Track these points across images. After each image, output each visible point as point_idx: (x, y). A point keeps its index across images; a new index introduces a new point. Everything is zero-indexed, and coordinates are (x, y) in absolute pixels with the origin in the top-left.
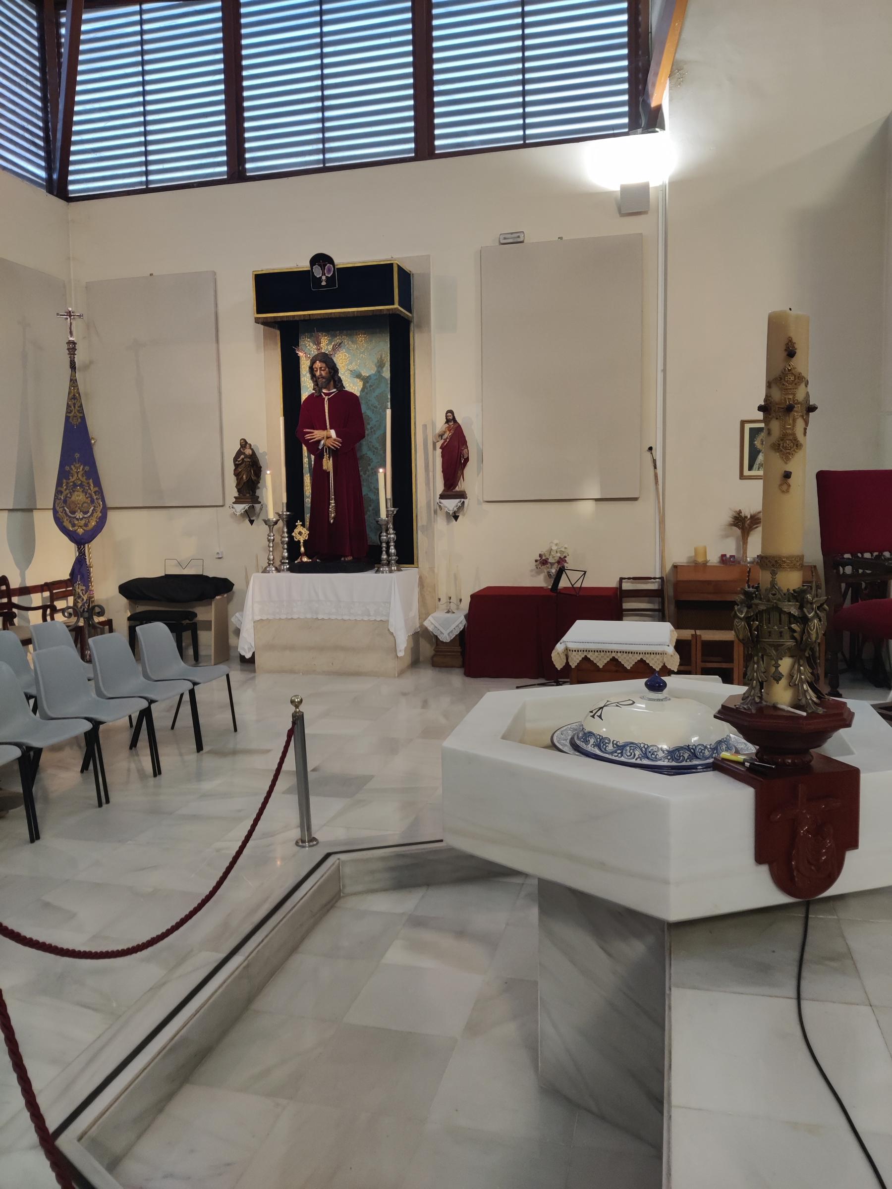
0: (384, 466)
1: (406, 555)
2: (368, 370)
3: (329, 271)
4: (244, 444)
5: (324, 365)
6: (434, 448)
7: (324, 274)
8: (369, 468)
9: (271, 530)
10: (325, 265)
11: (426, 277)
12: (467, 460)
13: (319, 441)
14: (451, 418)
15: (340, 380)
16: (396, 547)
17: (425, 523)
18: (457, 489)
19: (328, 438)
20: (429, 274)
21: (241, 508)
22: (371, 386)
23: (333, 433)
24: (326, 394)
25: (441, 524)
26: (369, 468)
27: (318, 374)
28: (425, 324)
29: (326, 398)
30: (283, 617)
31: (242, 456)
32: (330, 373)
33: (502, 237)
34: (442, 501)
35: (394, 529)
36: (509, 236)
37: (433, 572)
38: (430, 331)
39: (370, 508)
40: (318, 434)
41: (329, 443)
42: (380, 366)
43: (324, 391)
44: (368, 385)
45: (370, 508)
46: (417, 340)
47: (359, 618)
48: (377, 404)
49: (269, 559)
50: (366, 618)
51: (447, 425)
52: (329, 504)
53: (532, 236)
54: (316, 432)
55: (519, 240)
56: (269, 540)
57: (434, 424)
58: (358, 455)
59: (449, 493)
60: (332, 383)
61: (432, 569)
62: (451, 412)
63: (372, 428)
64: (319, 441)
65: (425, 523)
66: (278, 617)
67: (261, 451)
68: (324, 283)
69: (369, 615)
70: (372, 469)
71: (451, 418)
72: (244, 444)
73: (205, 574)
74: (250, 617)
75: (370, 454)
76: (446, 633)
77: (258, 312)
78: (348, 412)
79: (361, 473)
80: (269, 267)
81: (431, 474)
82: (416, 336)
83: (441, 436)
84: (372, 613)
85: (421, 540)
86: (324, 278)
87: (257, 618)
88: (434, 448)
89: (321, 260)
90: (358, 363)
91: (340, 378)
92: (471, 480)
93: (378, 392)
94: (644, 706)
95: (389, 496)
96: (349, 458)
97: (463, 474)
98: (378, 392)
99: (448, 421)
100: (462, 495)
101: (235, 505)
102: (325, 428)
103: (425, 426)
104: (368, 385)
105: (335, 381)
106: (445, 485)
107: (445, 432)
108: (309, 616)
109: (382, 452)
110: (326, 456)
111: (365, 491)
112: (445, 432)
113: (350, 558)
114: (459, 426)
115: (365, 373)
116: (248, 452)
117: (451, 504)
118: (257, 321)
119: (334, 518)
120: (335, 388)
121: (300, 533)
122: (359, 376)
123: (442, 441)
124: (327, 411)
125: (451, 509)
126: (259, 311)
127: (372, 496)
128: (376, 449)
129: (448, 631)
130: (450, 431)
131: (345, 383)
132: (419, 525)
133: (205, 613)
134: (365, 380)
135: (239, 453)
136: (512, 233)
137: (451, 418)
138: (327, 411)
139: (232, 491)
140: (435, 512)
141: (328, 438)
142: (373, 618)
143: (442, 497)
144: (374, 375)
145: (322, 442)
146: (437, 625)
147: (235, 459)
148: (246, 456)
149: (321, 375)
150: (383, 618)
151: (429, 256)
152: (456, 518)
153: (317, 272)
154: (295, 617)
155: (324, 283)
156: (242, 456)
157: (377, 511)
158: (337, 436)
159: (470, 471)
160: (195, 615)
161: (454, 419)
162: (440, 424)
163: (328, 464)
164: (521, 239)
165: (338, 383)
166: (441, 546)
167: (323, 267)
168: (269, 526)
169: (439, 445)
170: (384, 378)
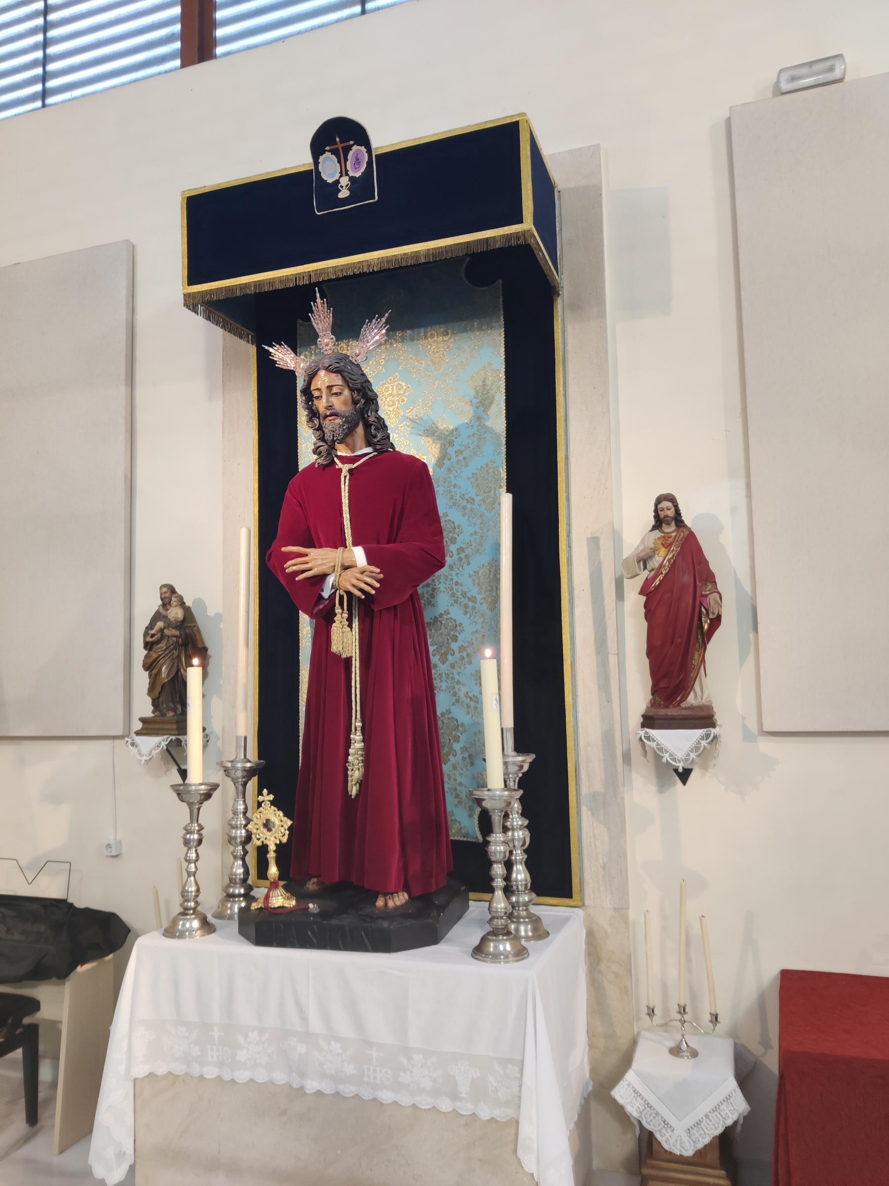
0: (496, 642)
1: (553, 873)
2: (453, 416)
3: (358, 161)
4: (169, 594)
5: (337, 380)
6: (620, 595)
7: (344, 172)
8: (454, 646)
9: (194, 816)
10: (347, 150)
11: (592, 196)
12: (716, 622)
13: (323, 577)
14: (667, 515)
15: (382, 425)
16: (528, 864)
17: (599, 787)
18: (691, 700)
19: (346, 568)
20: (600, 188)
21: (153, 744)
22: (458, 452)
23: (359, 555)
24: (344, 460)
25: (641, 791)
26: (454, 646)
27: (321, 405)
28: (592, 299)
29: (345, 468)
30: (210, 1072)
31: (160, 624)
32: (355, 402)
33: (784, 77)
34: (653, 733)
35: (524, 814)
36: (805, 70)
37: (625, 920)
38: (603, 315)
39: (457, 747)
40: (318, 559)
41: (350, 582)
42: (483, 403)
43: (342, 451)
44: (451, 451)
45: (457, 747)
46: (570, 337)
47: (425, 1102)
48: (472, 492)
49: (184, 894)
50: (445, 1105)
51: (657, 534)
52: (348, 743)
53: (861, 63)
54: (313, 553)
55: (830, 77)
56: (187, 842)
57: (617, 537)
58: (428, 616)
59: (671, 712)
60: (360, 430)
61: (621, 911)
62: (671, 498)
63: (460, 550)
64: (323, 577)
65: (599, 787)
66: (196, 1070)
67: (211, 613)
68: (344, 194)
69: (455, 1096)
70: (462, 648)
71: (671, 513)
72: (169, 594)
73: (70, 900)
74: (122, 1068)
75: (457, 614)
76: (680, 1126)
77: (191, 281)
78: (400, 507)
79: (434, 659)
80: (587, 876)
81: (612, 660)
82: (569, 329)
83: (644, 561)
84: (464, 1089)
85: (588, 832)
86: (345, 181)
87: (141, 1070)
88: (620, 595)
89: (340, 134)
90: (433, 394)
91: (380, 419)
92: (722, 675)
93: (475, 465)
94: (488, 652)
95: (509, 722)
96: (397, 616)
97: (703, 660)
98: (475, 465)
99: (659, 522)
100: (703, 719)
101: (139, 739)
102: (338, 542)
103: (594, 542)
104: (451, 451)
105: (367, 426)
106: (656, 690)
107: (654, 551)
108: (280, 1077)
109: (485, 607)
110: (341, 616)
111: (442, 702)
112: (654, 551)
113: (401, 899)
114: (691, 537)
115: (447, 423)
116: (175, 613)
117: (677, 743)
118: (191, 303)
119: (362, 783)
120: (369, 444)
121: (268, 825)
122: (431, 431)
123: (645, 575)
124: (345, 501)
125: (680, 755)
126: (192, 280)
127: (461, 715)
128: (473, 599)
129: (689, 1121)
130: (667, 546)
131: (394, 438)
132: (584, 790)
133: (57, 1004)
134: (446, 440)
135: (157, 617)
136: (810, 64)
137: (667, 515)
138: (345, 501)
139: (144, 707)
140: (627, 758)
141: (346, 568)
142: (466, 1108)
143: (649, 721)
144: (468, 426)
145: (330, 580)
146: (652, 1099)
147: (146, 634)
148: (169, 624)
149: (330, 407)
150: (499, 1113)
151: (598, 147)
152: (684, 775)
153: (329, 168)
154: (242, 1076)
155: (344, 194)
156: (160, 624)
157: (475, 755)
158: (370, 562)
159: (720, 652)
160: (34, 1005)
161: (678, 519)
162: (635, 528)
163: (346, 639)
164: (837, 74)
165: (376, 431)
166: (644, 848)
167: (341, 156)
168: (190, 805)
169: (639, 582)
170: (491, 431)
